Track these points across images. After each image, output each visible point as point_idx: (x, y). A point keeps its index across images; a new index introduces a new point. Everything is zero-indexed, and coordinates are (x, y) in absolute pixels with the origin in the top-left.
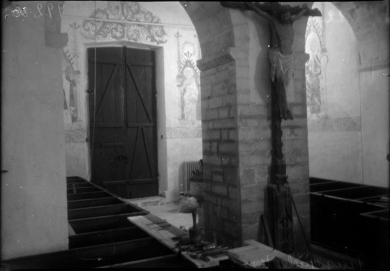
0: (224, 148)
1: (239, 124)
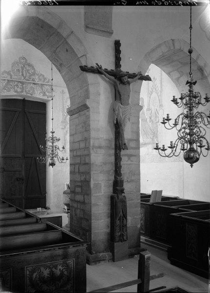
0: (82, 169)
1: (92, 151)
